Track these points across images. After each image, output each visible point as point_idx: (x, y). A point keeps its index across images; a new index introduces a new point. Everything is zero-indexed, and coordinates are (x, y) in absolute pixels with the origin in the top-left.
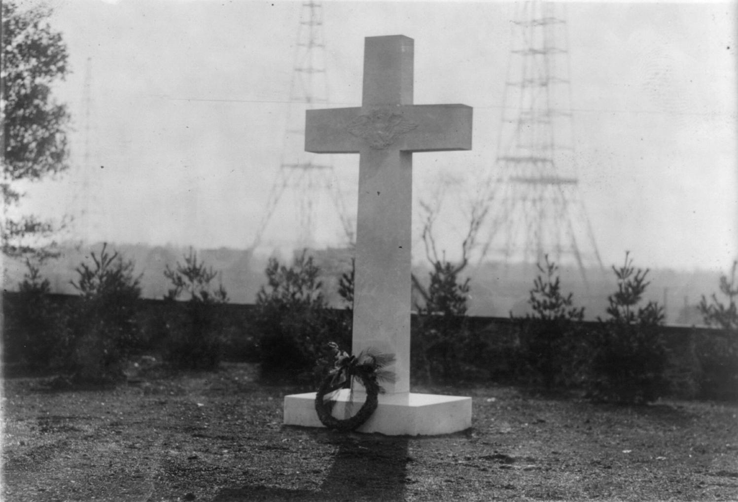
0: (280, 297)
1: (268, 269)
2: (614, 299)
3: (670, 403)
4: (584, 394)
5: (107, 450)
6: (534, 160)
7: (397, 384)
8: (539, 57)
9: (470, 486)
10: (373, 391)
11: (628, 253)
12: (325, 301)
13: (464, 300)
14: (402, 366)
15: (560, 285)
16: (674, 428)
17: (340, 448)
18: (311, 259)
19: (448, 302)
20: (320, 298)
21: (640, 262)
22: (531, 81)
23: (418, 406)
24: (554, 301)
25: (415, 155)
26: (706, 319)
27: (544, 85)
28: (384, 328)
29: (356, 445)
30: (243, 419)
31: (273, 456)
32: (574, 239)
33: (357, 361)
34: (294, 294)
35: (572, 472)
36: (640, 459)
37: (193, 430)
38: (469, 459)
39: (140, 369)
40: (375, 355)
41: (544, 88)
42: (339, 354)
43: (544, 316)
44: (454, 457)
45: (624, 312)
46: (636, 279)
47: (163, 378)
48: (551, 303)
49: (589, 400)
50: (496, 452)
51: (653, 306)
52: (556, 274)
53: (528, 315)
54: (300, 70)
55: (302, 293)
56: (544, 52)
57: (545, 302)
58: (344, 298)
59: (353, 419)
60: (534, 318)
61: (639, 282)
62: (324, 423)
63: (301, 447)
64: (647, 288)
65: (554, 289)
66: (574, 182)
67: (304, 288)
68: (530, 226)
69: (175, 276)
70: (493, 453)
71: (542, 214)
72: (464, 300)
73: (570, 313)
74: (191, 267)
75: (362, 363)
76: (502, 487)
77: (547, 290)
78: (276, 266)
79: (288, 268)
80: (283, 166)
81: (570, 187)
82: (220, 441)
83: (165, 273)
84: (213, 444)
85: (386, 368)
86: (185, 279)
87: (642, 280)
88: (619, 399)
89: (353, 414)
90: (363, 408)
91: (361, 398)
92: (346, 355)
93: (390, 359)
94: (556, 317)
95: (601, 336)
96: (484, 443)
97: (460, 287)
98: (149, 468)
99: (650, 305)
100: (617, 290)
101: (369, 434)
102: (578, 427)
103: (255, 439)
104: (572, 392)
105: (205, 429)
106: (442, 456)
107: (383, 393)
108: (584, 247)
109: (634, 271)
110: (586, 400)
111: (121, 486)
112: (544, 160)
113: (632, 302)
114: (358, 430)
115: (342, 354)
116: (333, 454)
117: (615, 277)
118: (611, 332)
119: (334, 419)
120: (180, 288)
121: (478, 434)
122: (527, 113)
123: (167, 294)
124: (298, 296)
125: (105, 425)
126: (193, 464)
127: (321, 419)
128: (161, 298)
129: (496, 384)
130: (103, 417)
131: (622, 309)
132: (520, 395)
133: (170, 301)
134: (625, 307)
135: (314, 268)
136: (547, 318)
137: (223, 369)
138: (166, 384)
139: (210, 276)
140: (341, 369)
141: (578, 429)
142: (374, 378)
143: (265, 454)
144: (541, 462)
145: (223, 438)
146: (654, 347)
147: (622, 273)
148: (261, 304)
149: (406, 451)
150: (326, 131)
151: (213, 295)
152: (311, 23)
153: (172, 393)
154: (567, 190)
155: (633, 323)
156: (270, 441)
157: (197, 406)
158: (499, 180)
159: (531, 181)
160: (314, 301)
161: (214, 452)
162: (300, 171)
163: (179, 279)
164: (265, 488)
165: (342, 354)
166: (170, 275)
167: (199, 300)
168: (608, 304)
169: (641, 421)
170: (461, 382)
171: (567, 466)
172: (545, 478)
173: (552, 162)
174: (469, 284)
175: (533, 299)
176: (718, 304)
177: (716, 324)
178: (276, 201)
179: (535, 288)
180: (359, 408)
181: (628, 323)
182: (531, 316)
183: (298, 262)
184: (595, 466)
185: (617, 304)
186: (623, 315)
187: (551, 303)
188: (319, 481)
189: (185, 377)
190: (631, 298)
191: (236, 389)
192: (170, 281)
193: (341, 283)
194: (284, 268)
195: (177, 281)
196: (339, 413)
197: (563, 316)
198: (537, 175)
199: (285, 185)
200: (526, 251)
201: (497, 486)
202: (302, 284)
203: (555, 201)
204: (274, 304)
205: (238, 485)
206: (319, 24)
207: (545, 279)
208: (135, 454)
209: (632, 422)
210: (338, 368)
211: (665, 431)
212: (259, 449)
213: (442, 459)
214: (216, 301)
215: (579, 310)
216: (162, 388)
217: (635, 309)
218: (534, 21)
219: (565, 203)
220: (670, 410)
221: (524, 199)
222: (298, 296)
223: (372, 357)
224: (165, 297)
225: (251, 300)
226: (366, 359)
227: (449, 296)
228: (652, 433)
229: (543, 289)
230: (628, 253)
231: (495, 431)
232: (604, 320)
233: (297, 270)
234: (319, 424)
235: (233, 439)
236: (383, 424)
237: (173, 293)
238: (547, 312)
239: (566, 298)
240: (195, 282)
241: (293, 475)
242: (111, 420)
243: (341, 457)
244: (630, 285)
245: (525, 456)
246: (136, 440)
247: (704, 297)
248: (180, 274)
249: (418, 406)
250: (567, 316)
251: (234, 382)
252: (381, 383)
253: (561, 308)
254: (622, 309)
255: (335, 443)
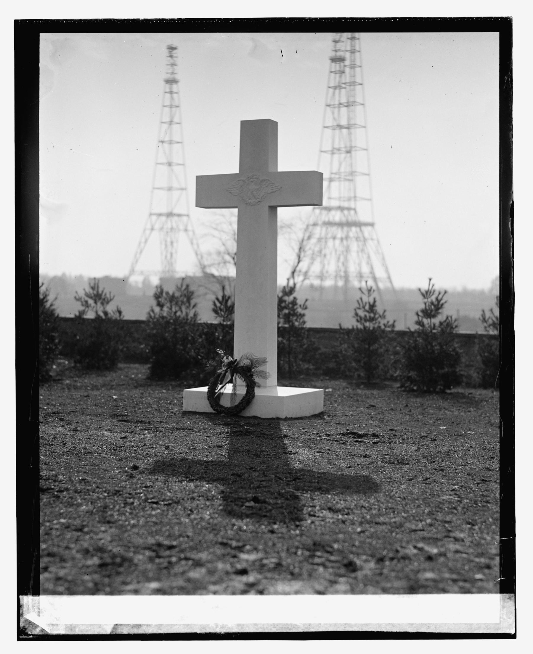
0: (165, 314)
1: (156, 294)
2: (420, 314)
3: (460, 390)
4: (398, 385)
5: (57, 432)
6: (341, 209)
7: (268, 381)
8: (345, 131)
9: (337, 456)
10: (251, 386)
11: (430, 280)
12: (199, 317)
13: (303, 315)
14: (272, 368)
15: (377, 304)
16: (472, 409)
17: (231, 428)
18: (188, 286)
19: (291, 317)
20: (195, 315)
21: (439, 285)
22: (339, 150)
23: (281, 396)
24: (372, 315)
25: (279, 209)
26: (485, 327)
27: (349, 152)
28: (256, 340)
29: (243, 426)
30: (151, 407)
31: (182, 435)
32: (372, 268)
33: (238, 363)
34: (176, 313)
35: (408, 444)
36: (456, 433)
37: (118, 416)
38: (329, 435)
39: (58, 370)
40: (252, 359)
41: (349, 155)
42: (225, 358)
43: (365, 327)
44: (317, 434)
45: (428, 324)
46: (437, 299)
47: (78, 377)
48: (370, 317)
49: (403, 389)
50: (348, 430)
51: (450, 318)
52: (375, 295)
53: (353, 326)
54: (162, 142)
55: (182, 312)
56: (348, 128)
57: (366, 316)
58: (216, 315)
59: (236, 406)
60: (357, 329)
61: (438, 301)
62: (214, 410)
63: (202, 428)
64: (445, 306)
65: (372, 307)
66: (372, 225)
67: (183, 308)
68: (339, 259)
69: (83, 300)
70: (345, 431)
71: (348, 250)
72: (303, 315)
73: (384, 325)
74: (95, 292)
75: (242, 364)
76: (361, 456)
77: (367, 307)
78: (162, 292)
79: (171, 293)
80: (151, 214)
81: (370, 228)
82: (140, 424)
83: (75, 298)
84: (136, 427)
85: (261, 368)
86: (91, 302)
87: (441, 300)
88: (425, 388)
89: (238, 401)
90: (244, 398)
91: (242, 391)
92: (230, 359)
93: (263, 362)
94: (374, 328)
95: (411, 342)
96: (337, 423)
97: (300, 306)
98: (94, 446)
99: (447, 318)
100: (423, 306)
101: (249, 417)
102: (401, 410)
103: (166, 422)
104: (387, 383)
105: (126, 415)
106: (309, 434)
107: (259, 386)
108: (380, 273)
109: (435, 293)
110: (399, 389)
111: (80, 460)
112: (349, 209)
113: (434, 316)
114: (241, 414)
115: (227, 358)
116: (227, 433)
117: (421, 297)
118: (418, 339)
119: (222, 406)
120: (87, 309)
121: (329, 416)
122: (335, 174)
123: (77, 314)
124: (179, 313)
125: (48, 413)
126: (126, 443)
127: (212, 407)
128: (72, 316)
129: (327, 378)
130: (45, 408)
131: (426, 321)
132: (349, 386)
133: (79, 319)
134: (429, 320)
135: (190, 292)
136: (367, 329)
137: (120, 369)
138: (81, 381)
139: (109, 299)
140: (227, 369)
141: (401, 412)
142: (252, 376)
143: (177, 434)
144: (383, 437)
145: (141, 422)
146: (451, 349)
147: (426, 294)
148: (151, 320)
149: (281, 430)
150: (211, 191)
151: (112, 314)
152: (171, 106)
153: (89, 388)
154: (367, 230)
155: (434, 331)
156: (177, 424)
157: (113, 398)
158: (315, 225)
159: (340, 225)
160: (191, 318)
161: (137, 433)
162: (163, 218)
163: (86, 302)
164: (187, 459)
165: (227, 358)
166: (78, 299)
167: (101, 317)
168: (416, 318)
169: (446, 404)
170: (302, 377)
171: (403, 439)
172: (391, 449)
173: (355, 209)
174: (307, 303)
175: (357, 314)
176: (494, 316)
177: (493, 331)
178: (146, 241)
179: (358, 306)
180: (241, 398)
181: (431, 331)
182: (355, 327)
183: (179, 289)
184: (424, 439)
185: (422, 317)
186: (427, 326)
187: (370, 317)
188: (224, 452)
189: (93, 376)
190: (433, 313)
191: (135, 384)
192: (79, 303)
193: (215, 304)
194: (167, 293)
195: (84, 303)
196: (226, 403)
197: (380, 327)
198: (344, 220)
199: (152, 229)
200: (336, 277)
201: (357, 455)
202: (182, 305)
203: (357, 239)
204: (161, 320)
205: (165, 458)
206: (177, 107)
207: (365, 299)
208: (80, 435)
209: (439, 406)
210: (224, 369)
211: (465, 412)
212: (171, 430)
213: (309, 436)
214: (114, 318)
215: (391, 322)
216: (79, 384)
217: (436, 321)
218: (340, 104)
219: (365, 240)
220: (463, 396)
221: (334, 238)
222: (179, 313)
223: (251, 360)
224: (76, 315)
225: (143, 317)
226: (246, 362)
227: (292, 312)
228: (456, 413)
229: (364, 307)
230: (430, 280)
231: (341, 414)
232: (412, 330)
233: (177, 294)
234: (210, 410)
235: (149, 422)
236: (257, 410)
237: (82, 313)
238: (367, 324)
239: (381, 313)
240: (99, 304)
241: (203, 449)
242: (52, 410)
243: (233, 435)
244: (432, 303)
245: (371, 433)
246: (76, 425)
247: (483, 311)
248: (86, 299)
249: (281, 396)
250: (383, 327)
251: (132, 379)
252: (256, 379)
253: (377, 321)
254: (426, 321)
255: (227, 425)
